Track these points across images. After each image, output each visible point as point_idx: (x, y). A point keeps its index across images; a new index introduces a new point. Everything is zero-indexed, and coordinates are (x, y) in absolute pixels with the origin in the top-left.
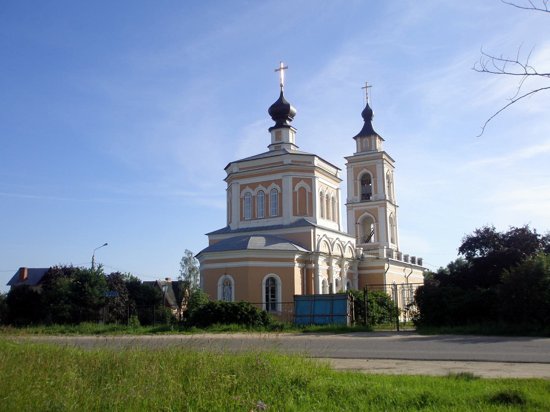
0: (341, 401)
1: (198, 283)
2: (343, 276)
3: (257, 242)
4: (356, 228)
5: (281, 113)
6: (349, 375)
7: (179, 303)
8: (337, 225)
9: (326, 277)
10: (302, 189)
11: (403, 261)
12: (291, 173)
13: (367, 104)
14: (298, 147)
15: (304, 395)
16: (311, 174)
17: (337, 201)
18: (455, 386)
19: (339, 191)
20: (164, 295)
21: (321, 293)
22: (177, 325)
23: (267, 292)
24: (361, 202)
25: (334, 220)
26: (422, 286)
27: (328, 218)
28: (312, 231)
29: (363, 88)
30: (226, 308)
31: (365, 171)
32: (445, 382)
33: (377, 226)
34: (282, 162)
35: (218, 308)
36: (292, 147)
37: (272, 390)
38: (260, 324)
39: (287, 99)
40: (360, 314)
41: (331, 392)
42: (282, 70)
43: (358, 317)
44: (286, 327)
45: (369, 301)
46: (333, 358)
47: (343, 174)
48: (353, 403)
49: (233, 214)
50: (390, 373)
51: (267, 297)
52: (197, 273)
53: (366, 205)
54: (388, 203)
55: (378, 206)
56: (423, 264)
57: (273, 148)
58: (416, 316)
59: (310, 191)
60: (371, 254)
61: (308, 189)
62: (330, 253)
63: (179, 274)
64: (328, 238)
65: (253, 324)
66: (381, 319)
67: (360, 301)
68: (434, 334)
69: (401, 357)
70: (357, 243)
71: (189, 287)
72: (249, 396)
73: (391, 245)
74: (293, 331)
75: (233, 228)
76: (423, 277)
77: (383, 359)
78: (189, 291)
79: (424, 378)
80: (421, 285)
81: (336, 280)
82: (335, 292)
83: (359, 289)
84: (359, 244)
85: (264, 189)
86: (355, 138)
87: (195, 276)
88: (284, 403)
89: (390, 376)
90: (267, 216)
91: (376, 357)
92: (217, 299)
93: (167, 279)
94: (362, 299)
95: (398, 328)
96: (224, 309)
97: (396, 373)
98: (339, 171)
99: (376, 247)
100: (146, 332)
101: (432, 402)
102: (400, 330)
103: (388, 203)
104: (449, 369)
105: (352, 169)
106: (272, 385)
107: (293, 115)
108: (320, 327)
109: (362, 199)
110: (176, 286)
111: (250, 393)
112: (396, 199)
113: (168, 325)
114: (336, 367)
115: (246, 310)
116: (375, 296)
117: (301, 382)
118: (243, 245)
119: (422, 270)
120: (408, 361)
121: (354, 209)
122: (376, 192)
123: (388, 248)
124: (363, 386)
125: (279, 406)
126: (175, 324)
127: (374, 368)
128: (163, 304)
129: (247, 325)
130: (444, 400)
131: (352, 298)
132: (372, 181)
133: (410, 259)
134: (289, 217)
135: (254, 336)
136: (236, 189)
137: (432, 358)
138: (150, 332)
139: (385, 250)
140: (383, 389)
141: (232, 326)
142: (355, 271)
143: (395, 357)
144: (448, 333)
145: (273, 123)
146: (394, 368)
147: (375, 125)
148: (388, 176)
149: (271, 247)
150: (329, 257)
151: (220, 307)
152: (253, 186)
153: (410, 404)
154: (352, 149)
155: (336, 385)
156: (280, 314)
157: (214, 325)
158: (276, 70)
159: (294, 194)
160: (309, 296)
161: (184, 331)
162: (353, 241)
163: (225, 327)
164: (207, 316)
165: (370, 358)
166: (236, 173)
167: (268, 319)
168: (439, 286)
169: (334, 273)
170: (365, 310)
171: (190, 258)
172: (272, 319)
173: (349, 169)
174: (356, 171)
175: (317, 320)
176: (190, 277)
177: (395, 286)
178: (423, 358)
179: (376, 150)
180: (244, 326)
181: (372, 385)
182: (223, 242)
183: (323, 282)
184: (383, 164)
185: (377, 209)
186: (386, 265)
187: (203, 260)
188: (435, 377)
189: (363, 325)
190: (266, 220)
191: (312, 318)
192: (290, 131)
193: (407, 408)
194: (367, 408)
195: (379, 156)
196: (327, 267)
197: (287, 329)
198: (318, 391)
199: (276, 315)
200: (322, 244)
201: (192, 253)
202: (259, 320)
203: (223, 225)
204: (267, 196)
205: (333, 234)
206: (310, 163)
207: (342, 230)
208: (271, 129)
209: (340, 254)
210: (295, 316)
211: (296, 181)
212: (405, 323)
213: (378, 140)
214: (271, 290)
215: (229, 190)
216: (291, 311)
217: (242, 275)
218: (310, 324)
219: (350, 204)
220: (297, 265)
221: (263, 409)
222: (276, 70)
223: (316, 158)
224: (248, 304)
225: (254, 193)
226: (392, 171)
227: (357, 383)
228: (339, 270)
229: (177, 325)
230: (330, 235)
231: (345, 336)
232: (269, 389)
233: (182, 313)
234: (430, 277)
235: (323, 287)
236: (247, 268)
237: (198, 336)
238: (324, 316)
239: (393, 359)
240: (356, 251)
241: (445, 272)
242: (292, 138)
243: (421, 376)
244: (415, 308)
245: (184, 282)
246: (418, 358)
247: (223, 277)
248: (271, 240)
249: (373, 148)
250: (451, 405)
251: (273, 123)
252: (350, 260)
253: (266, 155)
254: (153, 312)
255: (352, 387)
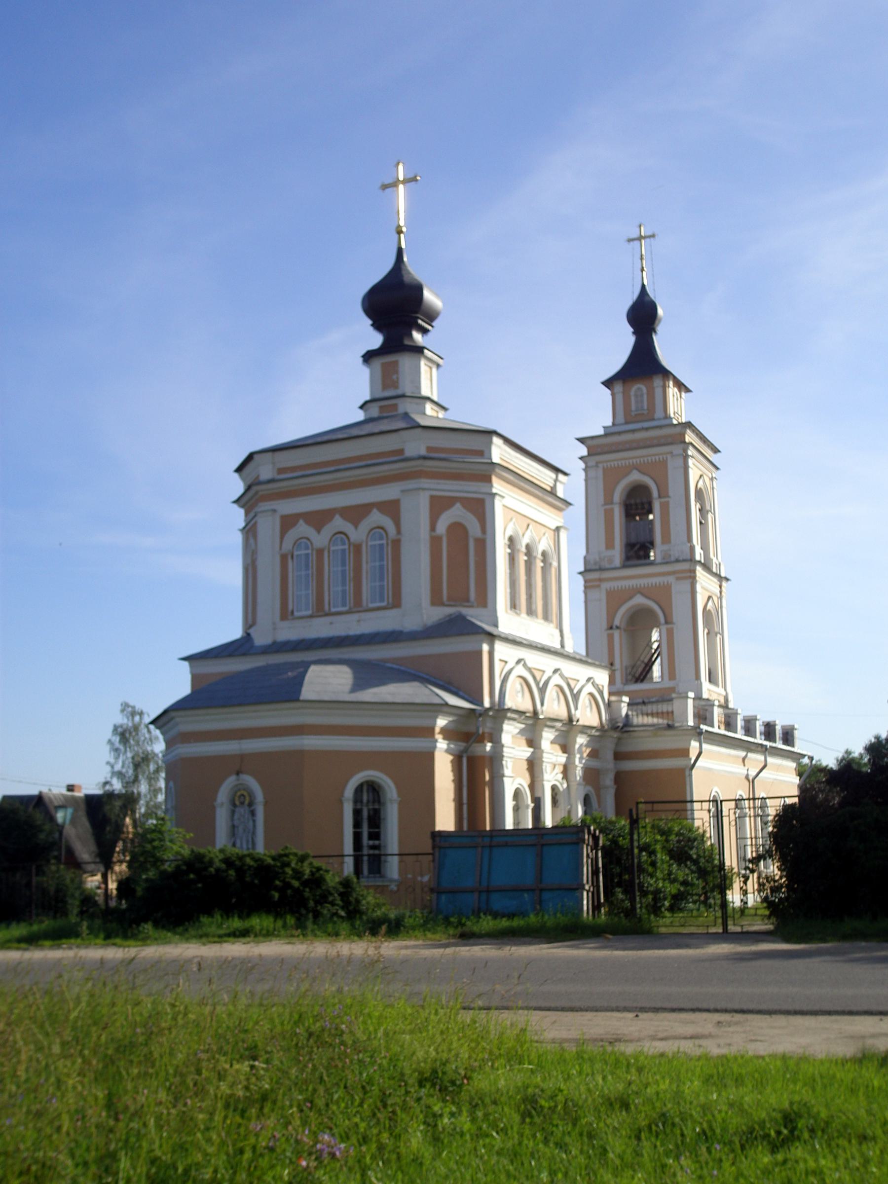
0: (558, 1132)
1: (161, 798)
2: (571, 778)
3: (327, 681)
4: (611, 639)
5: (397, 309)
6: (583, 1055)
7: (106, 860)
8: (557, 632)
9: (523, 781)
10: (458, 530)
11: (740, 735)
12: (425, 483)
13: (643, 286)
14: (444, 409)
15: (452, 1114)
16: (480, 487)
17: (555, 564)
18: (876, 1083)
19: (563, 534)
20: (61, 833)
21: (509, 825)
22: (98, 922)
23: (357, 824)
24: (624, 566)
25: (546, 617)
26: (792, 806)
27: (531, 612)
28: (485, 648)
29: (630, 240)
30: (241, 871)
31: (635, 477)
32: (851, 1076)
33: (670, 635)
34: (401, 451)
35: (218, 870)
36: (429, 409)
37: (361, 1105)
38: (336, 914)
39: (415, 269)
40: (619, 885)
41: (530, 1107)
42: (401, 187)
43: (613, 894)
44: (408, 921)
45: (645, 848)
46: (536, 1009)
47: (573, 486)
48: (591, 1136)
49: (260, 599)
50: (698, 1052)
51: (357, 837)
52: (157, 771)
53: (639, 577)
54: (699, 569)
55: (671, 579)
56: (797, 742)
57: (375, 411)
58: (774, 890)
59: (479, 534)
60: (652, 715)
61: (474, 528)
62: (535, 713)
63: (104, 773)
64: (530, 670)
65: (317, 915)
66: (678, 898)
67: (621, 848)
68: (823, 940)
69: (730, 1006)
70: (612, 682)
71: (133, 812)
72: (297, 1122)
73: (708, 690)
74: (429, 935)
75: (261, 639)
76: (796, 780)
77: (681, 1010)
78: (135, 822)
79: (791, 1063)
80: (789, 801)
81: (554, 788)
82: (549, 823)
83: (618, 813)
84: (619, 685)
85: (348, 528)
86: (608, 383)
87: (152, 779)
88: (398, 1137)
89: (699, 1058)
90: (357, 607)
91: (659, 1005)
92: (213, 844)
93: (71, 788)
94: (624, 842)
95: (725, 925)
96: (232, 872)
97: (716, 1051)
98: (561, 477)
99: (666, 696)
100: (9, 941)
101: (812, 1131)
102: (731, 928)
103: (699, 569)
104: (863, 1037)
105: (600, 472)
106: (363, 1087)
107: (431, 316)
108: (504, 923)
109: (628, 558)
110: (100, 811)
111: (301, 1111)
112: (720, 559)
113: (73, 919)
114: (549, 1035)
115: (298, 874)
116: (662, 833)
117: (446, 1078)
118: (288, 690)
119: (793, 760)
120: (750, 1017)
121: (605, 586)
122: (666, 539)
123: (698, 698)
124: (621, 1087)
125: (381, 1148)
126: (92, 917)
127: (654, 1038)
128: (58, 858)
129: (298, 919)
130: (845, 1126)
131: (596, 839)
132: (656, 506)
133: (759, 728)
134: (419, 609)
135: (319, 948)
136: (268, 527)
137: (816, 1008)
138: (20, 940)
139: (690, 702)
140: (678, 1095)
141: (255, 922)
142: (608, 763)
143: (712, 1007)
144: (864, 936)
145: (376, 340)
146: (709, 1036)
147: (664, 346)
148: (699, 493)
149: (370, 694)
150: (533, 724)
151: (223, 866)
152: (318, 519)
153: (750, 1137)
154: (598, 413)
155: (544, 1086)
156: (394, 887)
157: (204, 919)
158: (385, 187)
159: (435, 541)
160: (479, 832)
161: (117, 936)
162: (602, 677)
163: (236, 923)
164: (183, 894)
165: (643, 1010)
166: (270, 481)
167: (358, 901)
168: (842, 804)
169: (547, 767)
170: (631, 873)
171: (136, 728)
172: (369, 899)
173: (592, 473)
174: (611, 477)
175: (498, 902)
176: (136, 780)
177: (716, 802)
178: (790, 1008)
179: (667, 417)
180: (291, 920)
181: (646, 1086)
182: (232, 681)
183: (517, 794)
184: (686, 457)
185: (667, 588)
186: (694, 745)
187: (173, 733)
188: (822, 1062)
189: (626, 916)
190: (355, 617)
191: (484, 896)
192: (423, 363)
193: (743, 1147)
194: (629, 1151)
195: (675, 437)
196: (527, 752)
197: (413, 928)
198: (495, 1102)
199: (381, 890)
200: (513, 685)
201: (141, 714)
202: (333, 904)
203: (233, 631)
204: (358, 548)
205: (543, 660)
206: (481, 453)
207: (569, 648)
208: (369, 357)
209: (563, 713)
210: (437, 890)
211: (439, 505)
212: (743, 910)
213: (672, 390)
214: (369, 819)
215: (249, 531)
216: (426, 879)
217: (285, 773)
218: (477, 913)
219: (592, 572)
220: (442, 744)
221: (333, 1156)
222: (385, 187)
223: (496, 440)
224: (302, 859)
225: (320, 539)
226: (712, 479)
227: (604, 1078)
228: (562, 758)
229: (98, 922)
230: (535, 659)
231: (577, 947)
232: (353, 1099)
233: (113, 886)
234: (814, 779)
235: (516, 809)
236: (299, 755)
237: (151, 952)
238: (518, 889)
239: (708, 1010)
240: (609, 705)
241: (859, 764)
242: (429, 382)
243: (784, 1058)
244: (772, 868)
245: (119, 796)
246: (776, 1007)
247: (231, 780)
248: (368, 674)
249: (659, 414)
250: (863, 1138)
251: (376, 340)
252: (593, 732)
253: (355, 432)
254: (28, 884)
255: (589, 1090)
